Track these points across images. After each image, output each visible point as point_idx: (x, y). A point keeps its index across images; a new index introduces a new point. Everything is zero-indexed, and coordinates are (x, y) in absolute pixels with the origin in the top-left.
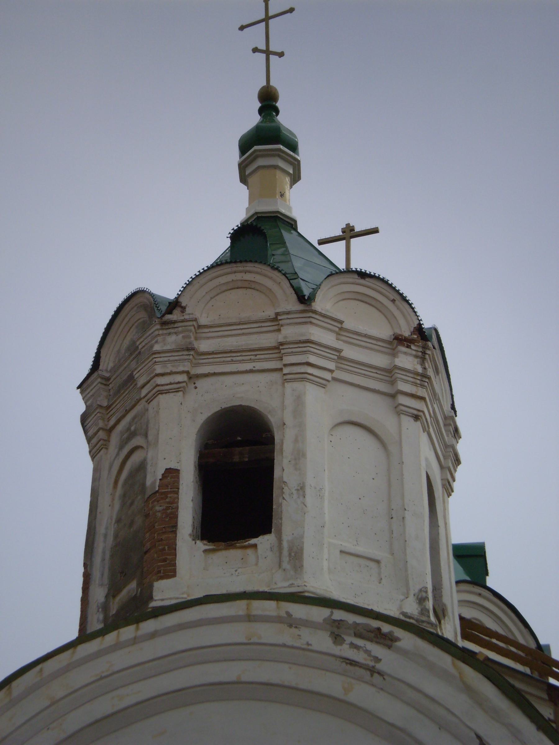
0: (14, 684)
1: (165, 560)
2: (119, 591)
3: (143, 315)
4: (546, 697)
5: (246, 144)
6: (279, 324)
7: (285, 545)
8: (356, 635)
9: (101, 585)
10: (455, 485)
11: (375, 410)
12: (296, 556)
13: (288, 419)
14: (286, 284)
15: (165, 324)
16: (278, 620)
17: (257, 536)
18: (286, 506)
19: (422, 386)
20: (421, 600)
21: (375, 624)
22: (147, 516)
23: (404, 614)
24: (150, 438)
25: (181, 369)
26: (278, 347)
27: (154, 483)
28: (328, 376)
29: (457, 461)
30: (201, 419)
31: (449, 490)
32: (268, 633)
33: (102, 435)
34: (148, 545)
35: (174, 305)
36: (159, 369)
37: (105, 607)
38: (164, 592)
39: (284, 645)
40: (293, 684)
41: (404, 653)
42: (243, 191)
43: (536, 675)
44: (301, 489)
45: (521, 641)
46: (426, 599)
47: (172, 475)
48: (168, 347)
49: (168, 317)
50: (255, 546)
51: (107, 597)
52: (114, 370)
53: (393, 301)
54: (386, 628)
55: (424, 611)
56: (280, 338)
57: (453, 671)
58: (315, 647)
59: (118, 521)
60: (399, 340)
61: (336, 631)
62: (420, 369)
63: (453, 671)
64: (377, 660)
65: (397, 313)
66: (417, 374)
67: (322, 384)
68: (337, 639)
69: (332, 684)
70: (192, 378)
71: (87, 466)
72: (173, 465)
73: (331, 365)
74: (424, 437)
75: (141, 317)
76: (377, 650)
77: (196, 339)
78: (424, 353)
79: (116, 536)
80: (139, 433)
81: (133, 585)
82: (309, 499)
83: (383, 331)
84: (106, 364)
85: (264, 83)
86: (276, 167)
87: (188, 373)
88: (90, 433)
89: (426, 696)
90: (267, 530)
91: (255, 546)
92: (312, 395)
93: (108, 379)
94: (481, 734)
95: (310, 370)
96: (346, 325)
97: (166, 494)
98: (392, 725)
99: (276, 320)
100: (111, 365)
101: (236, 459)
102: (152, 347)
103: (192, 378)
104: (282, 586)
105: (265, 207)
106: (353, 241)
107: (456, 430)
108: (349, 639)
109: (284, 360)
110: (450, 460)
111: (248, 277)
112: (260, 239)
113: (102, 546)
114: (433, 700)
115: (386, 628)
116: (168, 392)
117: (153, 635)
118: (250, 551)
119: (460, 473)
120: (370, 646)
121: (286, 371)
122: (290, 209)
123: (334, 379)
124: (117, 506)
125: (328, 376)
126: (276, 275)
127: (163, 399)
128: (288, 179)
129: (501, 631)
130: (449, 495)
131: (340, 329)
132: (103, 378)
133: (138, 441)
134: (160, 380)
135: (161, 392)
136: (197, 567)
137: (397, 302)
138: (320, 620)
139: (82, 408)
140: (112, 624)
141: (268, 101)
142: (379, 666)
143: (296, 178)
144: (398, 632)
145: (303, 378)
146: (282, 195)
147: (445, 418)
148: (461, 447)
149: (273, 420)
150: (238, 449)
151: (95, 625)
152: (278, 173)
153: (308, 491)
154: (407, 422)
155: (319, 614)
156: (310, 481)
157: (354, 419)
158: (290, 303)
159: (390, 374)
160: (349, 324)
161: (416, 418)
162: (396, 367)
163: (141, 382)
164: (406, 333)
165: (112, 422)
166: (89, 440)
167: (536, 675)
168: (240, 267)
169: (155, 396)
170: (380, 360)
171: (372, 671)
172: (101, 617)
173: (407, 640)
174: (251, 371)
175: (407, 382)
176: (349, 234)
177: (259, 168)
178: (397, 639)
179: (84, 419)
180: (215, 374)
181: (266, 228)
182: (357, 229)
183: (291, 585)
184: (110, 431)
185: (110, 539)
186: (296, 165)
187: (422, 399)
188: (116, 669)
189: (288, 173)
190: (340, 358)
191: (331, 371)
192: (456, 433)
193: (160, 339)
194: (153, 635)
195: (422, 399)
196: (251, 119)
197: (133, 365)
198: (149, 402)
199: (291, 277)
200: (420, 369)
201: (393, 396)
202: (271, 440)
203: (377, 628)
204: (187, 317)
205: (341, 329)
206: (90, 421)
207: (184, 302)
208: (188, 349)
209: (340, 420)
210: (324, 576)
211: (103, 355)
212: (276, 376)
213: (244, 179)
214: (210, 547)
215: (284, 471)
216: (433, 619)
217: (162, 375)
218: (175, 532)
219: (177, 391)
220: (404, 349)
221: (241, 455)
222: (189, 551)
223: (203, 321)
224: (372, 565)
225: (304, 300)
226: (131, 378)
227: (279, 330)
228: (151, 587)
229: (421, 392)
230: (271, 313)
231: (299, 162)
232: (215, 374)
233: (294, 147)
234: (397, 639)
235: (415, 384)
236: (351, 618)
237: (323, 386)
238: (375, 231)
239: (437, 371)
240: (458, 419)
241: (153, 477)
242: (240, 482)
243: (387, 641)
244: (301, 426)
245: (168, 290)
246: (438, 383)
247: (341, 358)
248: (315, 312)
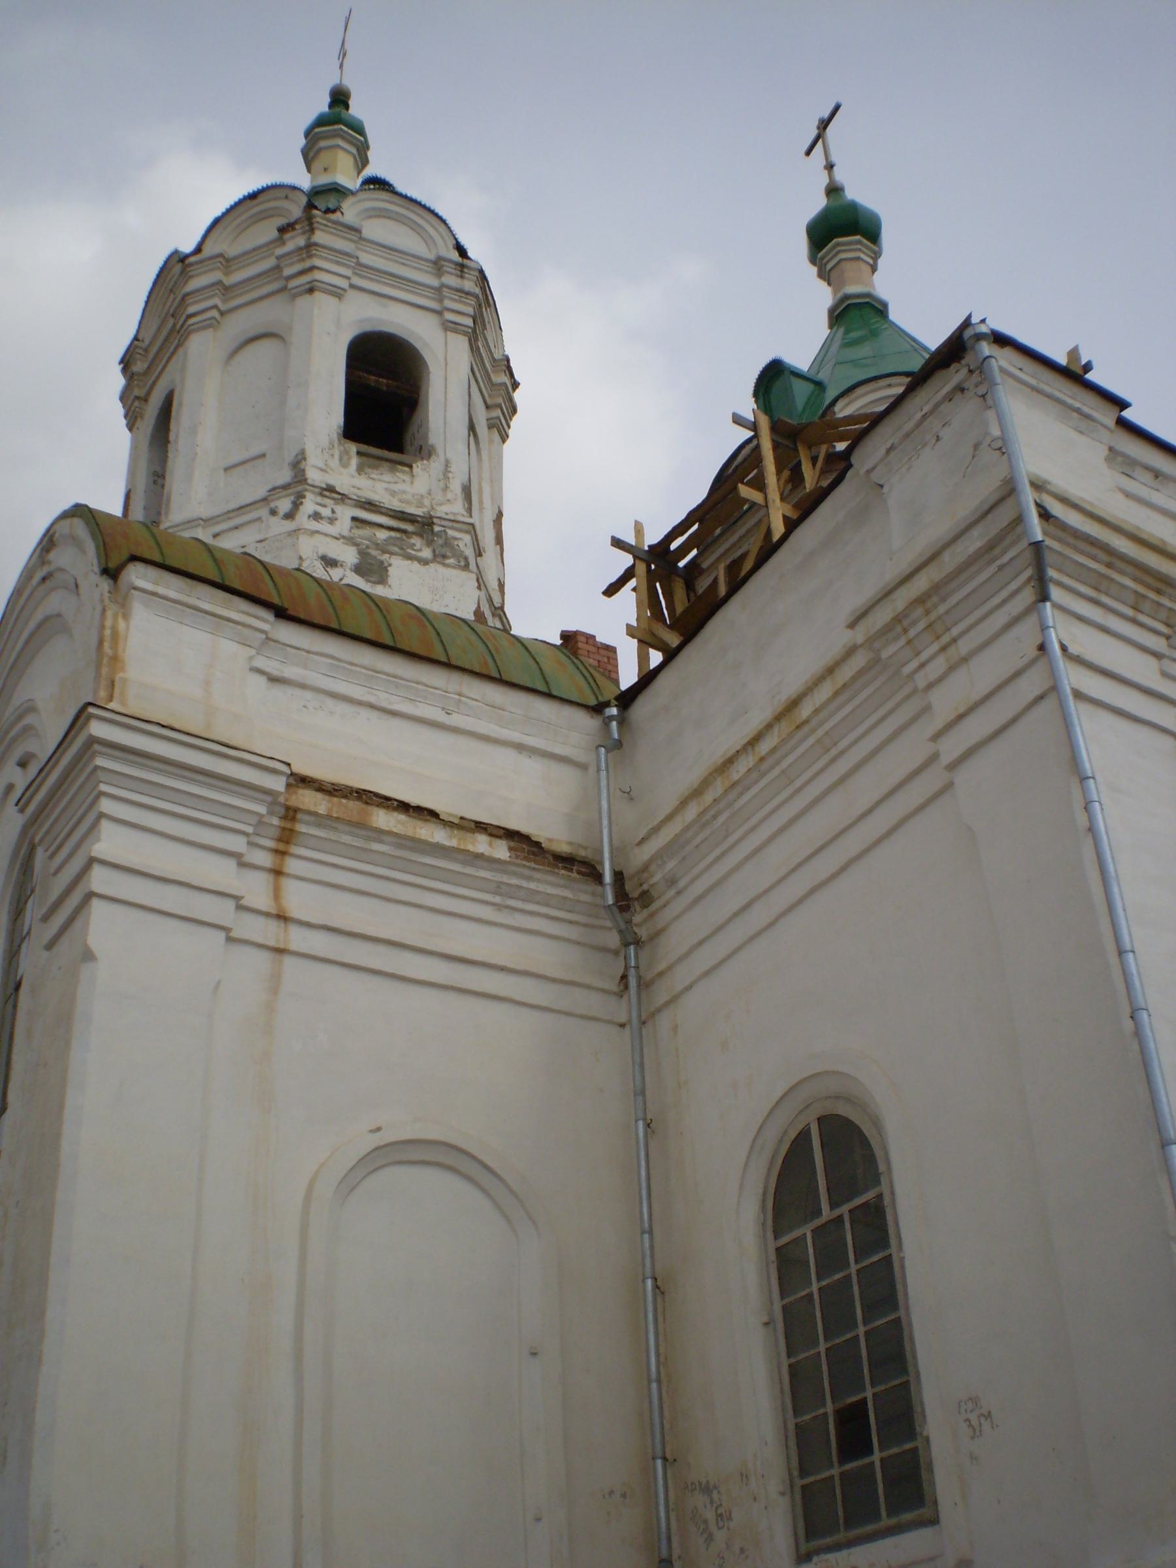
6: (915, 691)
73: (348, 272)
85: (827, 181)
86: (338, 146)
123: (952, 767)
125: (343, 283)
128: (869, 269)
130: (504, 442)
137: (290, 196)
177: (841, 260)
189: (867, 263)
190: (359, 264)
191: (348, 278)
237: (340, 297)
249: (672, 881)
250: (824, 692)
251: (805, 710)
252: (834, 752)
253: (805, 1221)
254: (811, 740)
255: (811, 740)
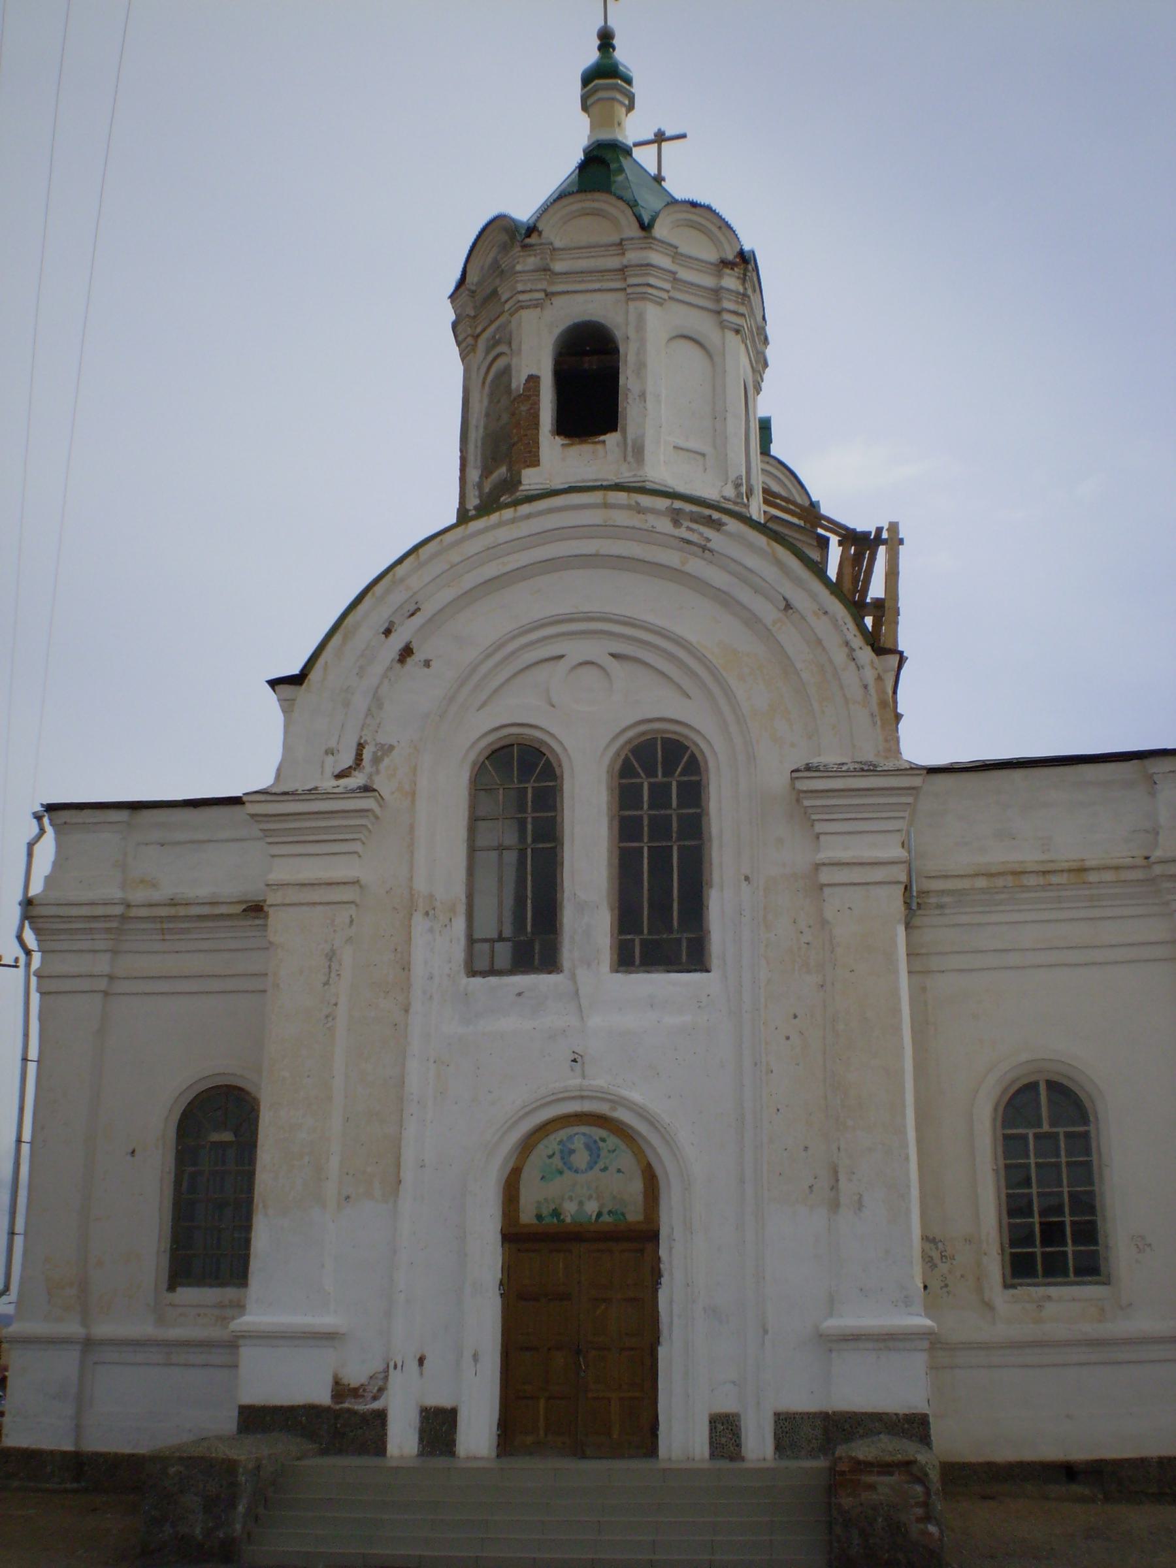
0: (421, 551)
1: (530, 452)
2: (491, 473)
3: (504, 237)
4: (815, 544)
5: (588, 78)
7: (629, 442)
8: (692, 520)
9: (476, 468)
10: (763, 385)
11: (703, 325)
12: (639, 452)
13: (632, 333)
14: (629, 212)
15: (525, 247)
16: (629, 507)
17: (605, 434)
18: (630, 409)
19: (743, 304)
20: (738, 486)
21: (707, 512)
22: (513, 414)
23: (725, 498)
24: (514, 347)
25: (540, 287)
26: (622, 271)
27: (518, 387)
28: (665, 296)
29: (766, 365)
30: (557, 331)
31: (758, 389)
32: (622, 518)
33: (470, 340)
34: (516, 439)
35: (532, 230)
36: (520, 287)
37: (480, 486)
38: (531, 479)
39: (633, 528)
40: (641, 557)
41: (730, 535)
42: (584, 121)
43: (808, 526)
44: (643, 396)
45: (799, 501)
46: (741, 485)
47: (533, 380)
48: (527, 268)
49: (528, 241)
50: (604, 442)
51: (481, 477)
52: (479, 284)
53: (720, 228)
54: (716, 515)
55: (739, 495)
56: (625, 261)
57: (766, 548)
58: (659, 529)
59: (487, 415)
60: (725, 263)
61: (676, 517)
62: (741, 290)
63: (766, 548)
64: (709, 540)
65: (722, 239)
66: (738, 293)
67: (660, 303)
68: (676, 523)
69: (671, 558)
70: (549, 295)
71: (458, 369)
72: (534, 372)
73: (667, 286)
74: (743, 347)
75: (503, 239)
76: (708, 532)
77: (552, 260)
78: (745, 275)
79: (486, 428)
80: (503, 341)
81: (503, 470)
82: (650, 404)
83: (712, 256)
84: (472, 278)
86: (613, 99)
87: (545, 291)
88: (460, 339)
89: (746, 567)
90: (614, 428)
91: (604, 442)
92: (652, 313)
93: (473, 292)
94: (788, 596)
95: (650, 290)
96: (680, 250)
97: (529, 397)
98: (719, 590)
99: (620, 246)
100: (475, 280)
101: (586, 366)
102: (514, 266)
103: (549, 295)
104: (626, 475)
105: (605, 136)
106: (663, 144)
107: (766, 339)
108: (686, 523)
109: (628, 281)
110: (760, 364)
111: (596, 205)
112: (601, 165)
113: (475, 436)
114: (751, 571)
115: (716, 515)
116: (528, 307)
117: (528, 516)
118: (599, 447)
119: (768, 374)
120: (702, 529)
121: (629, 290)
122: (626, 137)
123: (670, 298)
124: (486, 402)
125: (665, 296)
126: (620, 204)
127: (525, 314)
128: (624, 110)
129: (784, 493)
131: (675, 253)
132: (469, 290)
133: (502, 348)
134: (522, 297)
135: (522, 308)
136: (557, 460)
138: (663, 509)
139: (453, 317)
140: (489, 505)
141: (606, 40)
142: (709, 545)
143: (630, 108)
144: (725, 518)
145: (643, 297)
146: (619, 124)
147: (758, 328)
148: (770, 352)
149: (619, 334)
150: (587, 359)
151: (473, 502)
152: (617, 107)
153: (649, 397)
154: (730, 335)
155: (662, 503)
156: (650, 389)
157: (686, 333)
158: (633, 231)
159: (716, 293)
160: (684, 249)
161: (737, 332)
162: (722, 288)
163: (504, 298)
164: (730, 256)
165: (479, 330)
166: (458, 343)
167: (808, 526)
168: (589, 196)
169: (516, 311)
170: (708, 281)
171: (704, 548)
172: (477, 493)
173: (732, 525)
174: (599, 290)
175: (730, 300)
176: (660, 138)
177: (599, 100)
178: (724, 524)
179: (455, 326)
180: (567, 292)
181: (608, 156)
182: (668, 134)
183: (635, 476)
184: (476, 337)
185: (481, 430)
186: (631, 98)
187: (743, 315)
188: (501, 541)
189: (622, 104)
190: (675, 279)
191: (668, 291)
192: (766, 341)
193: (521, 260)
194: (528, 516)
195: (743, 315)
196: (591, 55)
197: (497, 281)
198: (511, 315)
199: (633, 205)
200: (741, 290)
201: (719, 313)
202: (615, 351)
203: (709, 513)
204: (543, 241)
205: (676, 253)
206: (459, 328)
207: (540, 226)
208: (545, 270)
209: (674, 334)
210: (662, 469)
211: (468, 270)
212: (620, 296)
213: (585, 108)
214: (566, 441)
215: (628, 379)
216: (745, 500)
217: (523, 292)
218: (537, 429)
219: (536, 306)
220: (728, 271)
221: (590, 363)
222: (549, 444)
223: (558, 244)
224: (699, 457)
225: (646, 227)
226: (494, 293)
227: (623, 254)
228: (519, 474)
229: (742, 309)
230: (615, 238)
231: (634, 95)
232: (567, 292)
233: (629, 81)
234: (724, 524)
235: (737, 302)
236: (688, 507)
237: (661, 304)
238: (683, 136)
239: (754, 291)
240: (767, 328)
241: (518, 382)
242: (590, 387)
243: (717, 525)
244: (642, 341)
245: (523, 213)
246: (755, 299)
247: (675, 280)
248: (655, 239)
249: (941, 906)
250: (1108, 876)
251: (1093, 877)
252: (1096, 903)
253: (1033, 1127)
254: (1087, 892)
255: (1087, 892)
